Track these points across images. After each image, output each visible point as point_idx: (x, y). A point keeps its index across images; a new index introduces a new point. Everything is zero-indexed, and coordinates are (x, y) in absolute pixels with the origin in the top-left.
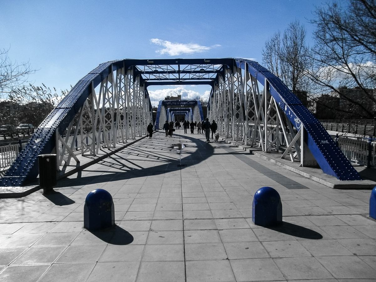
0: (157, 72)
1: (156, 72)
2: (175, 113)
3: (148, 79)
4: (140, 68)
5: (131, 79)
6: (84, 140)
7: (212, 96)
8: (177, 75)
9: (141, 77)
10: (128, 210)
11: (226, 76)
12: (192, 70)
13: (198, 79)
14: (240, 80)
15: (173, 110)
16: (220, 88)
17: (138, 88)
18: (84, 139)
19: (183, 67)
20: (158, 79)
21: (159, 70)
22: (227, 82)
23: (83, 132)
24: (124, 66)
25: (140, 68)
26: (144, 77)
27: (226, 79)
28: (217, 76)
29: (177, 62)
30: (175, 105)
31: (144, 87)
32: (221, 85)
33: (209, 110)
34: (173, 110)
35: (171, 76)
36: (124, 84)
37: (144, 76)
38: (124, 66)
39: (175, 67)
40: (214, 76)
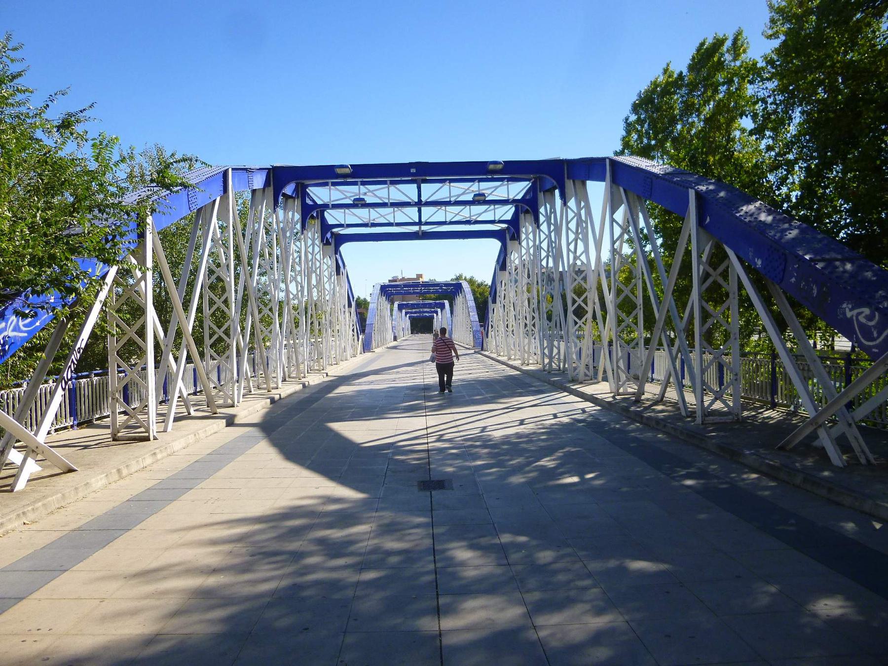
0: (363, 202)
1: (359, 203)
2: (411, 313)
3: (341, 226)
4: (319, 194)
5: (547, 256)
6: (211, 371)
7: (502, 264)
8: (412, 213)
9: (323, 220)
10: (386, 215)
11: (542, 210)
12: (453, 199)
13: (468, 222)
14: (552, 221)
15: (406, 306)
16: (524, 244)
17: (317, 249)
18: (213, 369)
19: (429, 191)
20: (365, 225)
21: (369, 200)
22: (544, 227)
23: (211, 356)
24: (272, 183)
25: (319, 194)
26: (331, 221)
27: (542, 219)
28: (516, 215)
29: (413, 170)
30: (410, 294)
31: (332, 247)
32: (527, 238)
33: (494, 301)
34: (406, 306)
35: (401, 215)
36: (540, 230)
37: (332, 216)
38: (272, 183)
39: (408, 191)
40: (506, 211)
